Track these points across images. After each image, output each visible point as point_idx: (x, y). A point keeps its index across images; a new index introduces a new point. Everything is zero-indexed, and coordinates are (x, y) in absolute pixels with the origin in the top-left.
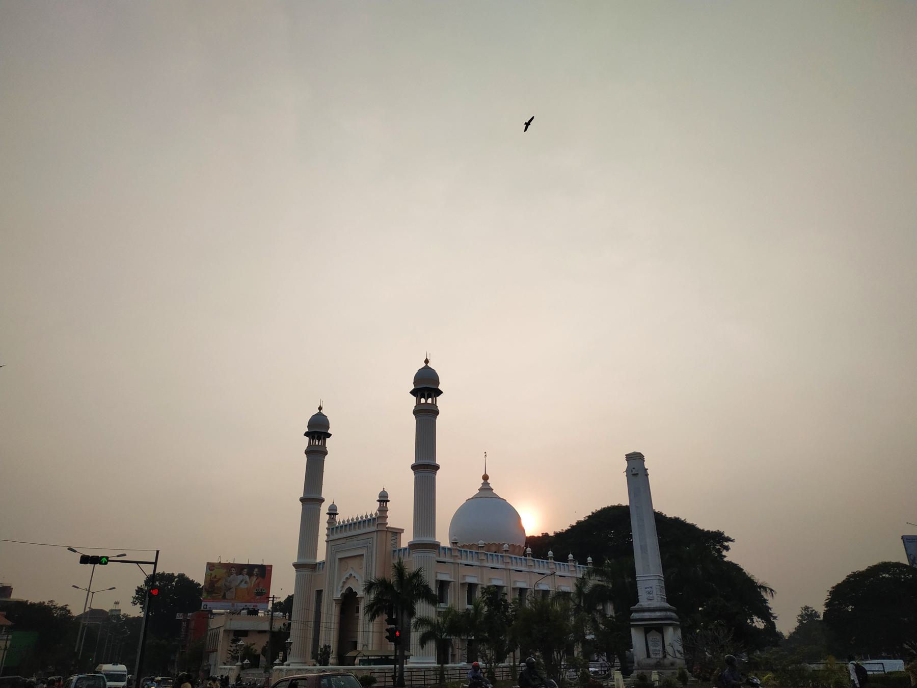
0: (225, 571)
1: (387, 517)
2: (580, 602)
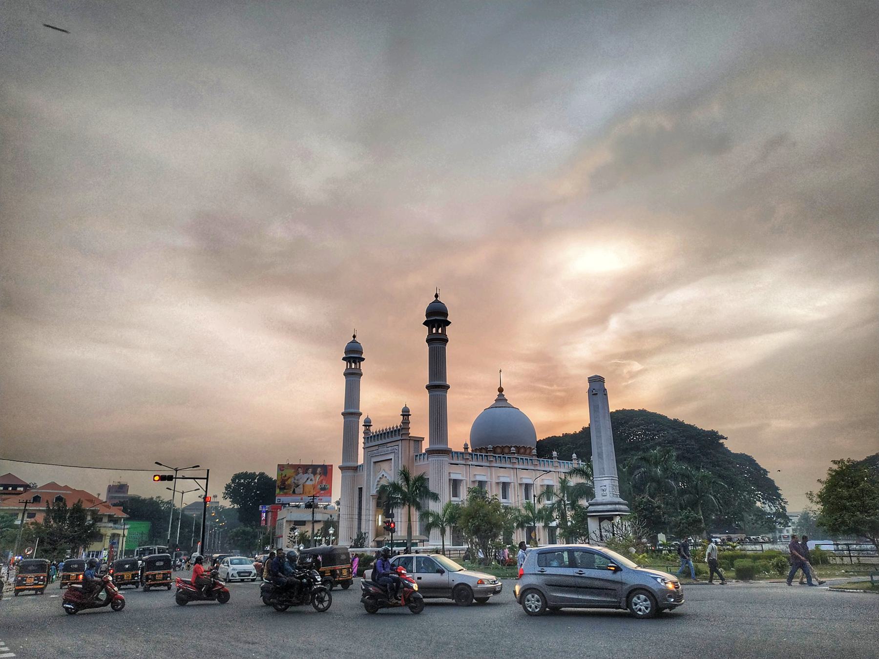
0: (293, 470)
1: (409, 428)
2: (563, 496)
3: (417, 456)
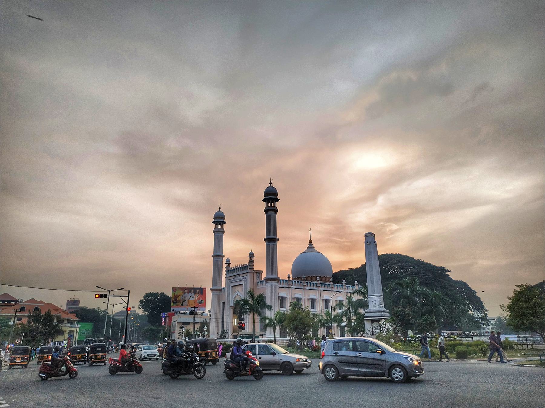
0: (182, 291)
1: (254, 265)
2: (349, 307)
3: (258, 282)
